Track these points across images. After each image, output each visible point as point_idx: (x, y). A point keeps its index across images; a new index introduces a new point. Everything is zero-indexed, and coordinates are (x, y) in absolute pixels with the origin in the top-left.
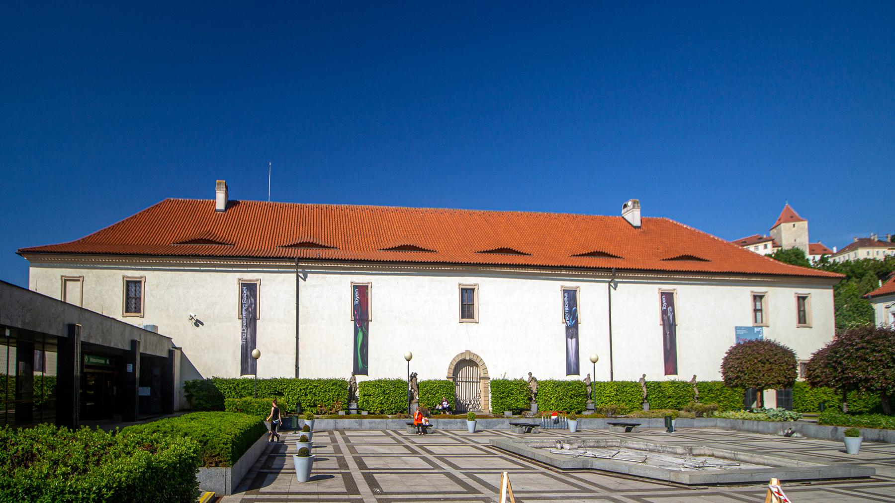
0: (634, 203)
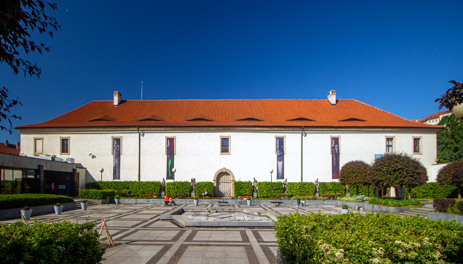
0: (332, 92)
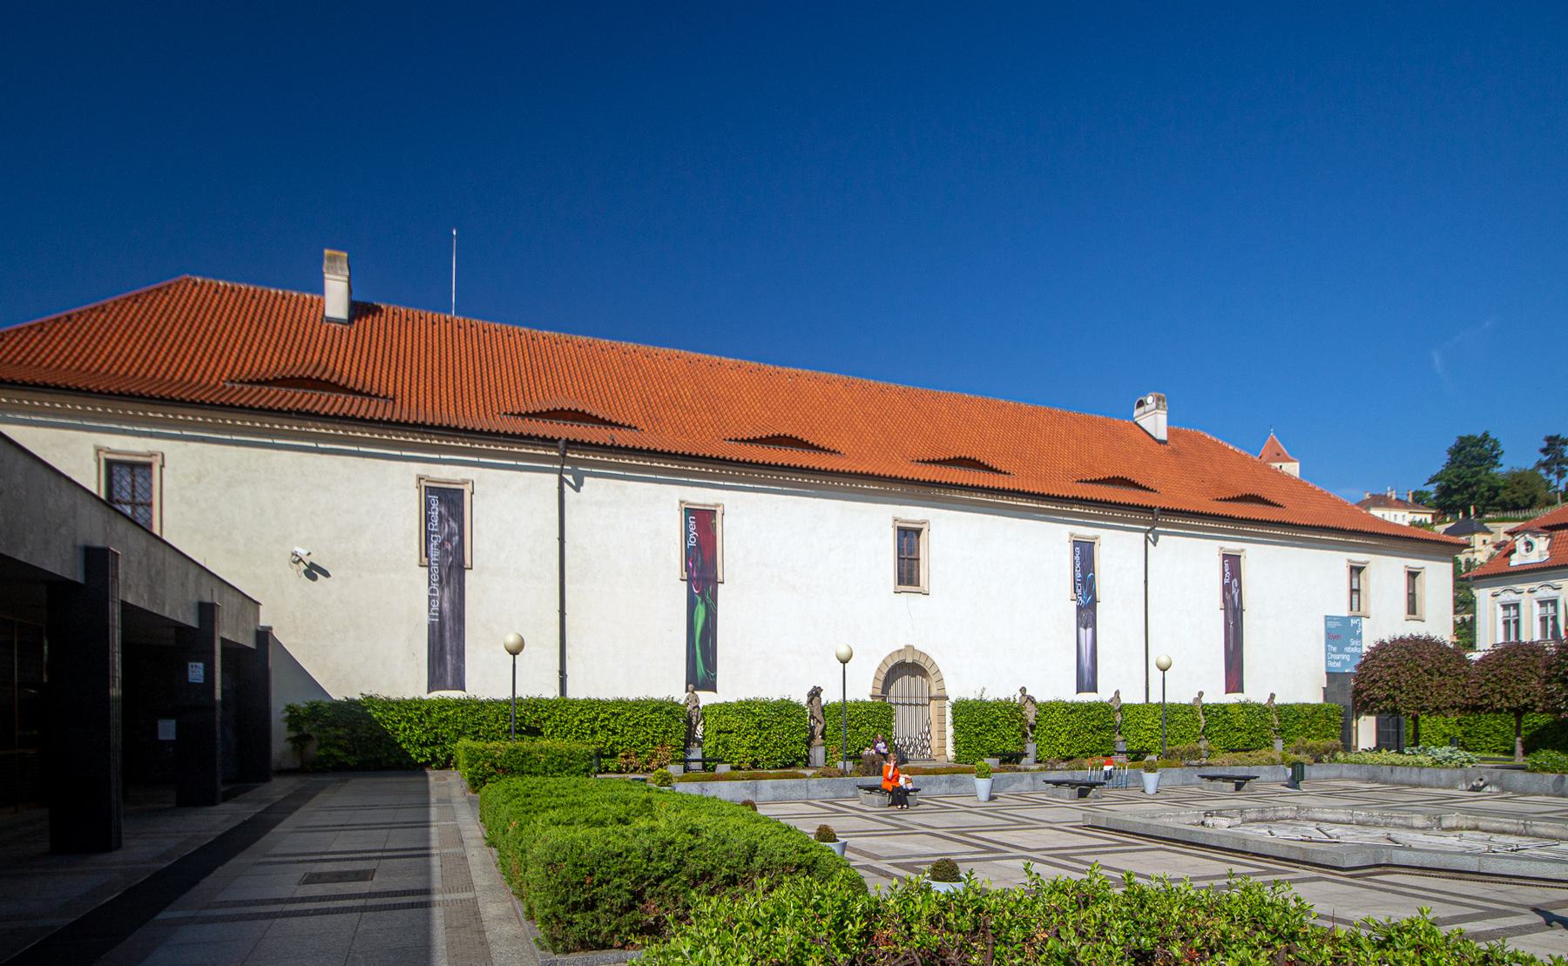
0: (1158, 399)
